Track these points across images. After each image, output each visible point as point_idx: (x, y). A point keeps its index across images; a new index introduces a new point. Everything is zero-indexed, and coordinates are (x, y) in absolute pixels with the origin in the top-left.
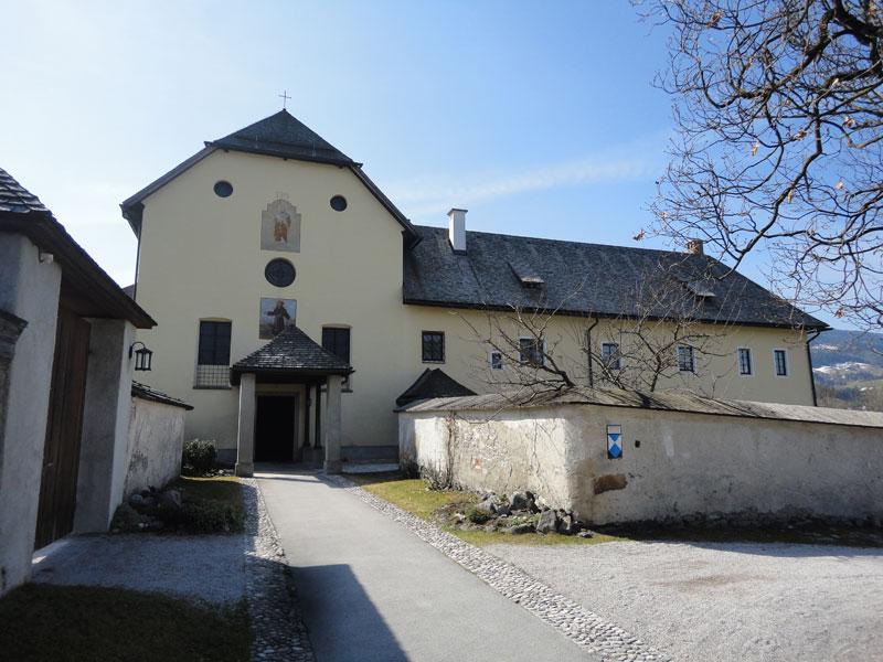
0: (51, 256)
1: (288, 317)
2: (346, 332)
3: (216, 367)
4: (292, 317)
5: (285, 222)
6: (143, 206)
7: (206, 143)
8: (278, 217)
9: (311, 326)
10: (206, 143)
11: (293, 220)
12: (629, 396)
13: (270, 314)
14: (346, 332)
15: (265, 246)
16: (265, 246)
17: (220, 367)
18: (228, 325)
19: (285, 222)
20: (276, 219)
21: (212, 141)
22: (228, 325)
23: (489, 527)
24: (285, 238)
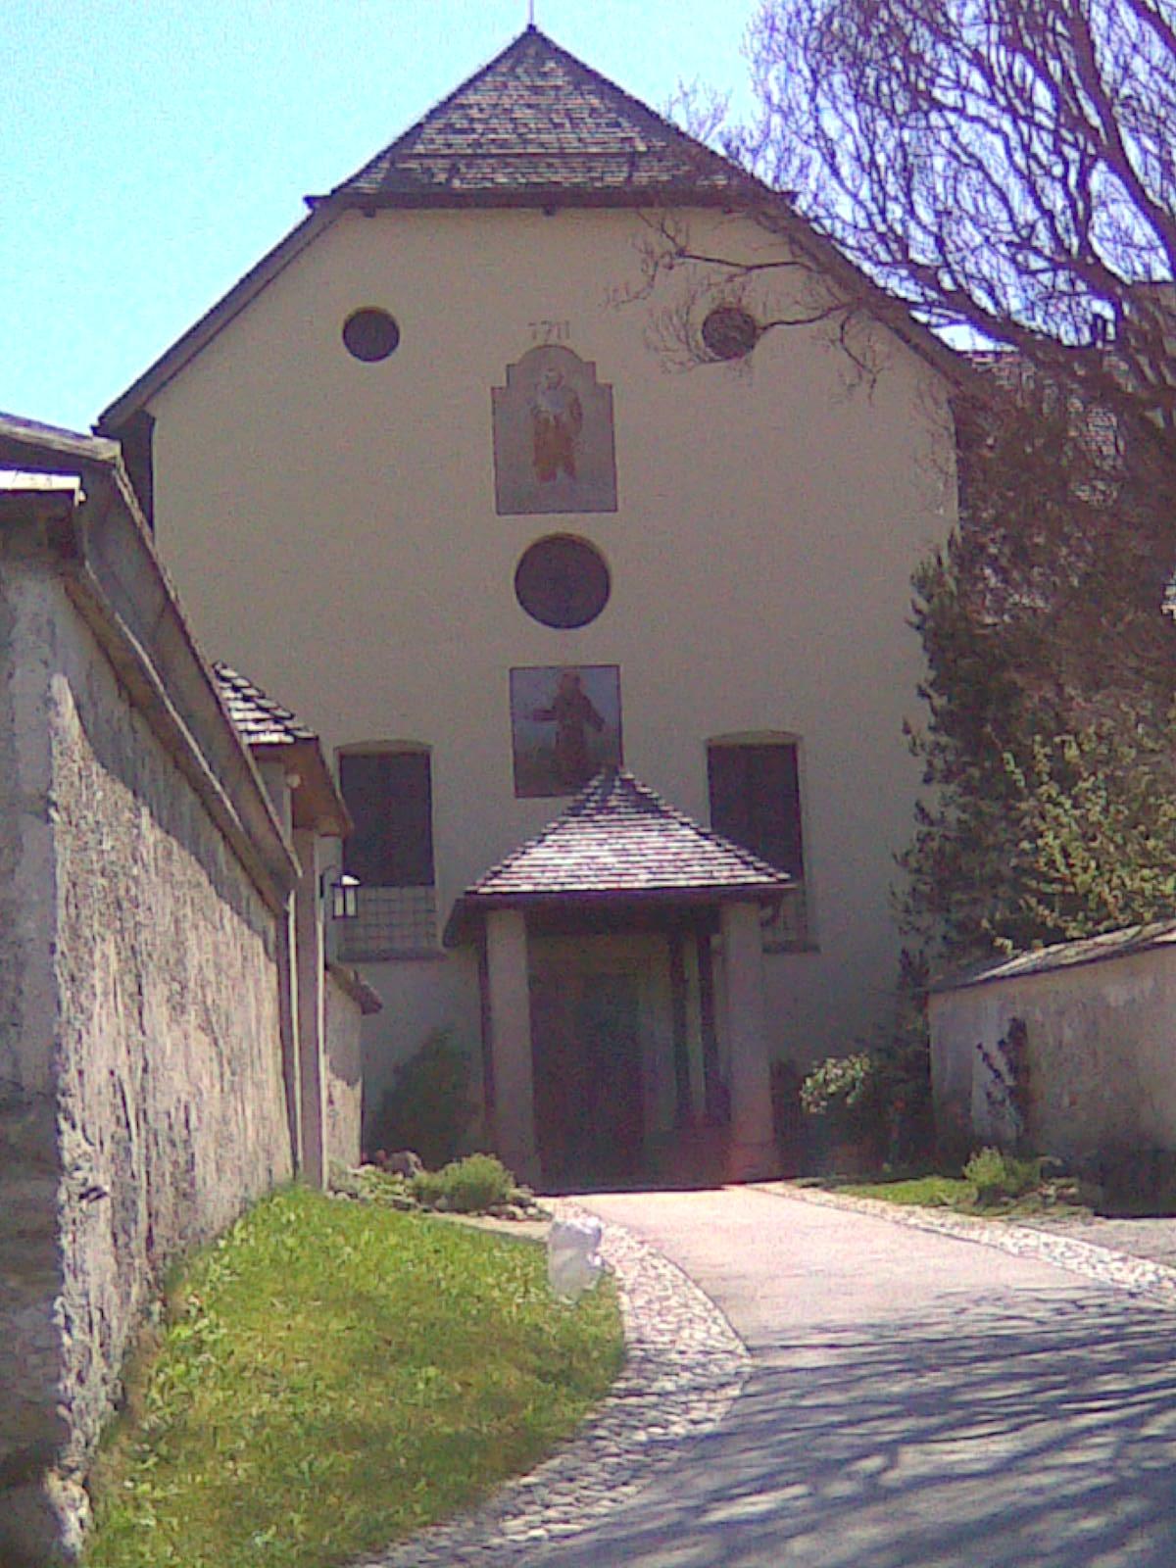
0: (1066, 342)
1: (599, 723)
2: (784, 755)
3: (394, 892)
4: (610, 720)
5: (565, 418)
6: (152, 421)
7: (309, 200)
8: (544, 404)
9: (933, 720)
10: (309, 200)
11: (588, 407)
12: (1033, 884)
13: (545, 715)
14: (784, 755)
15: (509, 502)
16: (509, 502)
17: (408, 892)
18: (418, 761)
19: (565, 418)
20: (536, 412)
21: (325, 191)
22: (418, 761)
23: (228, 1223)
24: (570, 469)
